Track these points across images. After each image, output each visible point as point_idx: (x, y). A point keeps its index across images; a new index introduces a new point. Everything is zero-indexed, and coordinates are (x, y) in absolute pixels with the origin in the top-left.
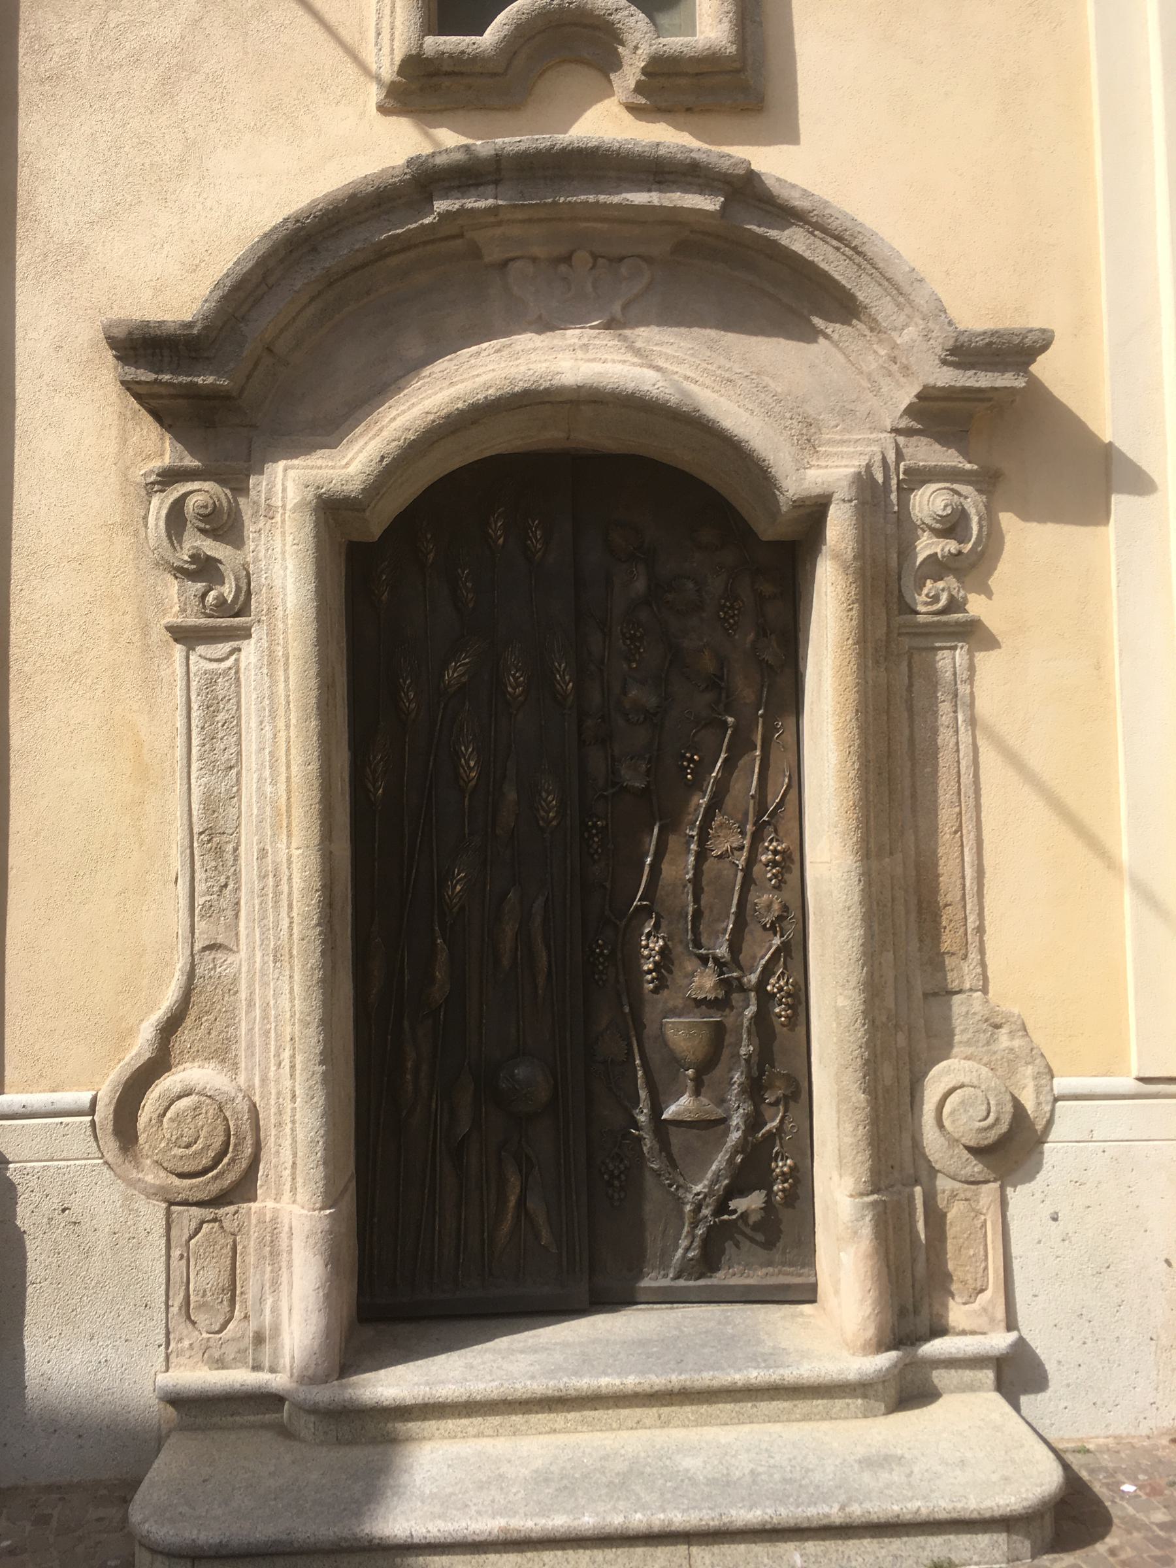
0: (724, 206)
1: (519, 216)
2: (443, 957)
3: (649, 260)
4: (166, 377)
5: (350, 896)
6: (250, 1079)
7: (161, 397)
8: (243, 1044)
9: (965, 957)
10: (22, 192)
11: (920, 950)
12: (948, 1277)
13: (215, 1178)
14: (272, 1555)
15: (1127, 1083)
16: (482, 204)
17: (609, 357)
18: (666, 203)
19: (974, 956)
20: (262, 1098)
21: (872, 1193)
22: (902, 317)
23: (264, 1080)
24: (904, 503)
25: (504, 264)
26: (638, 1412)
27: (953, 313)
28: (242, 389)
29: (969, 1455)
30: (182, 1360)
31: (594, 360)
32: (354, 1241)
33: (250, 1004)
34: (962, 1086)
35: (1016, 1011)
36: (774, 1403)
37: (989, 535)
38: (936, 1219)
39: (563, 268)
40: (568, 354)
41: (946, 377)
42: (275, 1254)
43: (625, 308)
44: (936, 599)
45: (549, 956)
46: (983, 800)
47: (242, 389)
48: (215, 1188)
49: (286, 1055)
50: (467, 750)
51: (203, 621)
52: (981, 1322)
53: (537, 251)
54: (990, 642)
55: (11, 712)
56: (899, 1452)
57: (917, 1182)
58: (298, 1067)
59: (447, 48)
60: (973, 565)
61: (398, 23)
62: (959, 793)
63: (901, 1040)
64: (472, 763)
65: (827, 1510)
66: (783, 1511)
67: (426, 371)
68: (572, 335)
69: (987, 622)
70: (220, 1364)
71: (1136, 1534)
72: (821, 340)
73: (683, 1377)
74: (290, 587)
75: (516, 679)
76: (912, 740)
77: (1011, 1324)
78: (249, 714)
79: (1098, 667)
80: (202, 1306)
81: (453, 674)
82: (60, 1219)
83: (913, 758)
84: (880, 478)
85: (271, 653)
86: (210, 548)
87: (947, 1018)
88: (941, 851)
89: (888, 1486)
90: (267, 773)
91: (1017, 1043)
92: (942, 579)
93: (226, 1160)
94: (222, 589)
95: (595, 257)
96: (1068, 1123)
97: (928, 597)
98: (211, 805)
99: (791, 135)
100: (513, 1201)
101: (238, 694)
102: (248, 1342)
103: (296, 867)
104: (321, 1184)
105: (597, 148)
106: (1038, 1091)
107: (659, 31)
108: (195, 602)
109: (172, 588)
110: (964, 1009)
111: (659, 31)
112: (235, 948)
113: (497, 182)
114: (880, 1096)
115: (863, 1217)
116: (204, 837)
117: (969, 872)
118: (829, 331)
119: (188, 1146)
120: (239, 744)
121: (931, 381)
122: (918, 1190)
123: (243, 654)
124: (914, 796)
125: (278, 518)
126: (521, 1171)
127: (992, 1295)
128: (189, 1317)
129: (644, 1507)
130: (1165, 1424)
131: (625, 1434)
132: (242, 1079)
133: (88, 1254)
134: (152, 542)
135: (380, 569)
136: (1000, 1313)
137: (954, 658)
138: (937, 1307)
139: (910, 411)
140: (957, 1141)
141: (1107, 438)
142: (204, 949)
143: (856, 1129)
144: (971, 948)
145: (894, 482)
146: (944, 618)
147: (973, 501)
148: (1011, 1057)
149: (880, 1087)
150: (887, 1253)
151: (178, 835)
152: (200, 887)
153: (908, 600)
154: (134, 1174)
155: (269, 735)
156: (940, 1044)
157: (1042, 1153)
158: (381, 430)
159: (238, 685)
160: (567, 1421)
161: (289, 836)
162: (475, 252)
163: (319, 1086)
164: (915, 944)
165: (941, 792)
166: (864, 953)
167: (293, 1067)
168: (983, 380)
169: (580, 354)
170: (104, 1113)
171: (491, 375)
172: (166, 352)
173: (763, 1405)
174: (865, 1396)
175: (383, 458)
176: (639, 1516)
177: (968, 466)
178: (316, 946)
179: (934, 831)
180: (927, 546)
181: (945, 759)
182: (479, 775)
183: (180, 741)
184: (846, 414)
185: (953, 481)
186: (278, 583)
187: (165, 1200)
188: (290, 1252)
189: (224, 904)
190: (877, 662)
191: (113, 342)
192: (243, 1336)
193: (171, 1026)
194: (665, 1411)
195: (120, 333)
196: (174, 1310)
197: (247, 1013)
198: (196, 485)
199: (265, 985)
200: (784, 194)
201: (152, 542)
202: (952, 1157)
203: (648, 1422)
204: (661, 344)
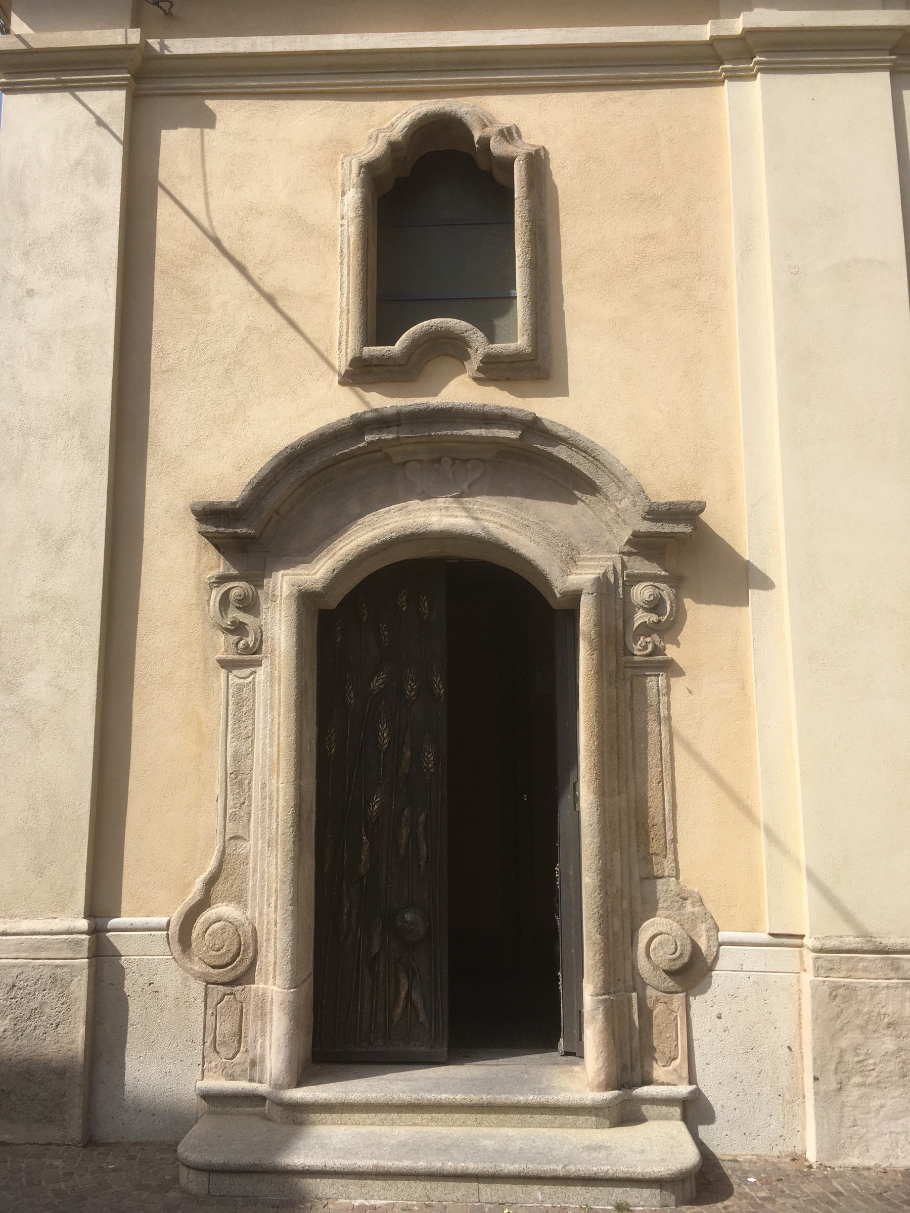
0: (521, 435)
1: (411, 441)
2: (366, 848)
3: (483, 461)
4: (222, 530)
5: (314, 810)
6: (253, 913)
7: (219, 538)
8: (250, 894)
9: (665, 857)
10: (151, 430)
11: (638, 851)
12: (654, 1049)
13: (232, 969)
14: (251, 1172)
15: (764, 937)
16: (390, 437)
17: (459, 514)
18: (490, 435)
19: (670, 856)
20: (259, 924)
21: (604, 994)
22: (621, 494)
23: (261, 914)
24: (627, 593)
25: (405, 463)
26: (464, 1116)
27: (649, 491)
28: (261, 535)
29: (648, 1148)
30: (211, 1074)
31: (450, 516)
32: (311, 1012)
33: (255, 870)
34: (661, 933)
35: (696, 890)
36: (543, 1116)
37: (677, 611)
38: (646, 1013)
39: (436, 465)
40: (437, 513)
41: (646, 527)
42: (263, 1014)
43: (470, 486)
44: (645, 648)
45: (427, 847)
46: (676, 764)
47: (261, 535)
48: (232, 975)
49: (273, 900)
50: (383, 727)
51: (236, 657)
52: (673, 1078)
53: (422, 457)
54: (680, 672)
55: (134, 705)
56: (609, 1144)
57: (635, 990)
58: (279, 907)
59: (375, 353)
60: (669, 627)
61: (350, 340)
62: (661, 759)
63: (625, 904)
64: (385, 735)
65: (556, 1167)
66: (531, 1166)
67: (360, 521)
68: (441, 502)
69: (678, 661)
70: (232, 1077)
71: (744, 1201)
72: (579, 502)
73: (489, 1097)
74: (283, 640)
75: (411, 687)
76: (633, 727)
77: (692, 1080)
78: (259, 708)
79: (743, 688)
80: (223, 1043)
81: (377, 683)
82: (148, 989)
83: (633, 739)
84: (612, 580)
85: (272, 674)
86: (242, 617)
87: (654, 893)
88: (650, 793)
89: (594, 1159)
90: (268, 741)
91: (696, 909)
92: (650, 636)
93: (238, 959)
94: (247, 639)
95: (453, 459)
96: (728, 959)
97: (640, 648)
98: (237, 758)
99: (562, 390)
100: (403, 994)
101: (254, 696)
102: (247, 1065)
103: (281, 793)
104: (289, 974)
105: (452, 408)
106: (709, 939)
107: (491, 339)
108: (233, 646)
109: (221, 639)
110: (665, 888)
111: (491, 339)
112: (246, 837)
113: (398, 426)
114: (610, 937)
115: (598, 1008)
116: (233, 776)
117: (667, 806)
118: (584, 498)
119: (218, 950)
120: (254, 724)
121: (637, 529)
122: (634, 995)
123: (257, 675)
124: (634, 760)
125: (278, 602)
126: (408, 976)
127: (680, 1062)
128: (215, 1049)
129: (453, 1160)
130: (789, 1150)
131: (455, 1128)
132: (249, 913)
133: (162, 1010)
134: (211, 614)
135: (335, 630)
136: (685, 1073)
137: (658, 681)
138: (646, 1068)
139: (628, 542)
140: (658, 966)
141: (747, 557)
142: (231, 838)
143: (595, 956)
144: (668, 851)
145: (621, 582)
146: (651, 658)
147: (666, 592)
148: (693, 917)
149: (610, 931)
150: (613, 1030)
151: (219, 775)
152: (230, 803)
153: (630, 648)
154: (189, 965)
155: (269, 720)
156: (650, 908)
157: (711, 977)
158: (334, 554)
159: (254, 692)
160: (423, 1119)
161: (278, 776)
162: (388, 458)
163: (289, 918)
164: (634, 848)
165: (650, 759)
166: (600, 852)
167: (276, 907)
168: (667, 528)
169: (444, 512)
170: (174, 929)
171: (394, 525)
172: (222, 517)
173: (537, 1117)
174: (597, 1116)
175: (334, 570)
176: (450, 1163)
177: (663, 573)
178: (291, 838)
179: (645, 781)
180: (641, 617)
181: (652, 740)
182: (390, 742)
183: (222, 722)
184: (594, 543)
185: (655, 582)
186: (277, 636)
187: (205, 981)
188: (271, 1013)
189: (242, 813)
190: (610, 683)
191: (195, 512)
192: (245, 1062)
193: (211, 882)
194: (480, 1116)
195: (199, 508)
196: (208, 1044)
197: (253, 875)
198: (236, 584)
199: (263, 860)
200: (554, 429)
201: (211, 614)
202: (655, 976)
203: (469, 1123)
204: (489, 506)
